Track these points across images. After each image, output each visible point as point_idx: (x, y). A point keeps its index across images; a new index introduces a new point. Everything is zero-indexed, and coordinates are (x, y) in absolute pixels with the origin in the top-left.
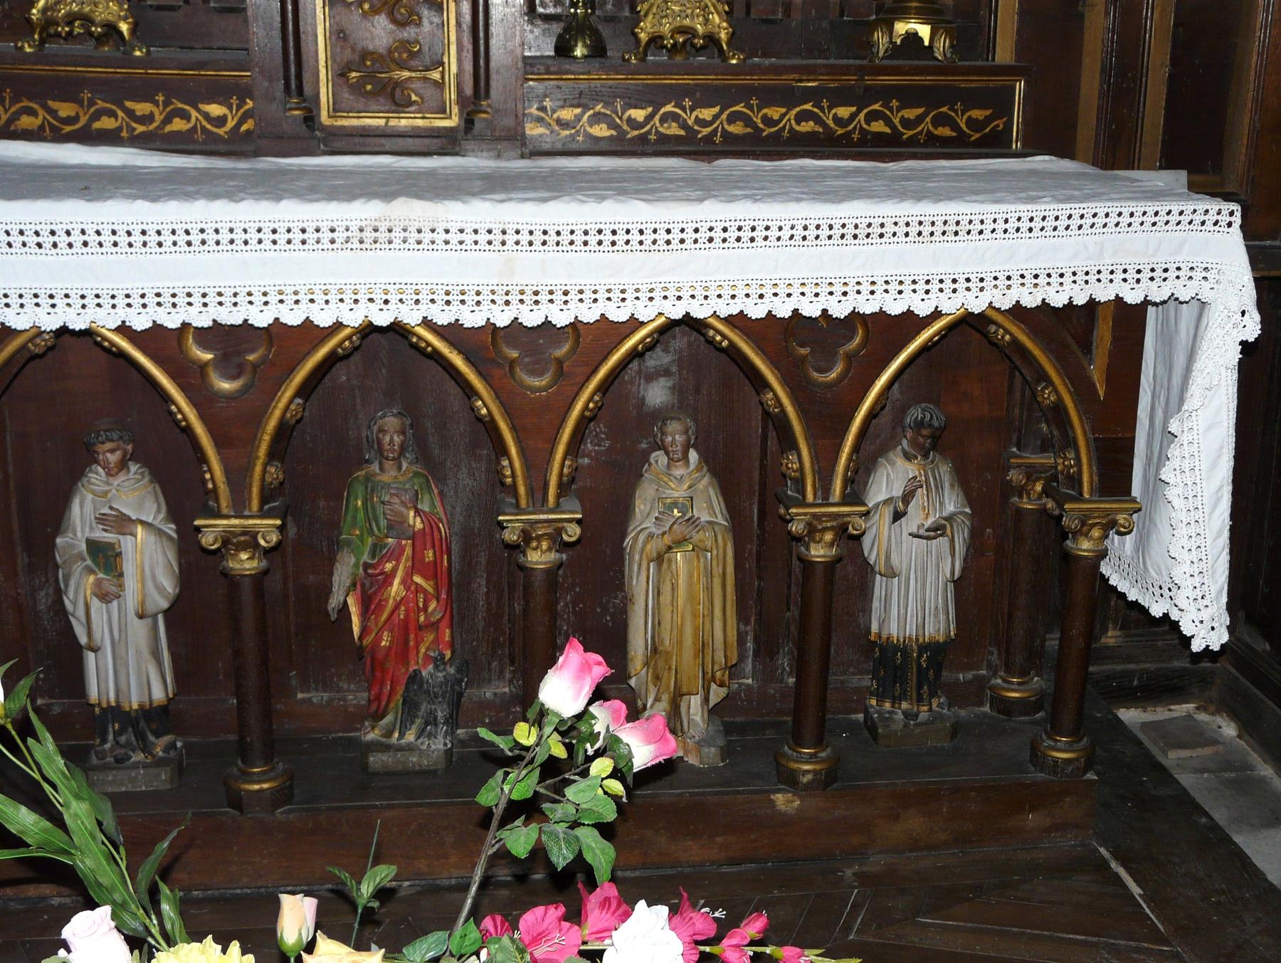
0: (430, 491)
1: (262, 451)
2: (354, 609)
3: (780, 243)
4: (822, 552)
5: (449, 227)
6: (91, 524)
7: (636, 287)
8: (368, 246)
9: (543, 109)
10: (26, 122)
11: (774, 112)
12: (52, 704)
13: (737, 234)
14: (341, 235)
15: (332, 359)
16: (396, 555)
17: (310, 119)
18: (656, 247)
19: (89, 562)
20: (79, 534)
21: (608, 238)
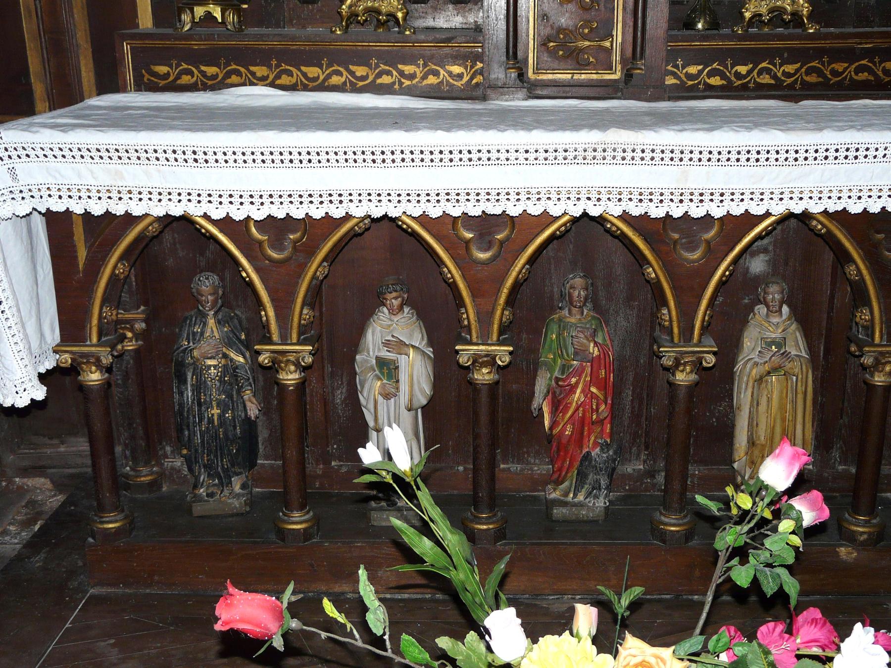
0: (602, 330)
1: (299, 301)
2: (546, 409)
3: (876, 160)
4: (883, 379)
5: (528, 149)
6: (379, 347)
7: (771, 191)
8: (589, 162)
10: (335, 80)
11: (839, 67)
12: (341, 466)
13: (846, 153)
14: (571, 154)
16: (579, 373)
17: (521, 76)
18: (787, 163)
19: (377, 372)
20: (371, 353)
21: (754, 156)
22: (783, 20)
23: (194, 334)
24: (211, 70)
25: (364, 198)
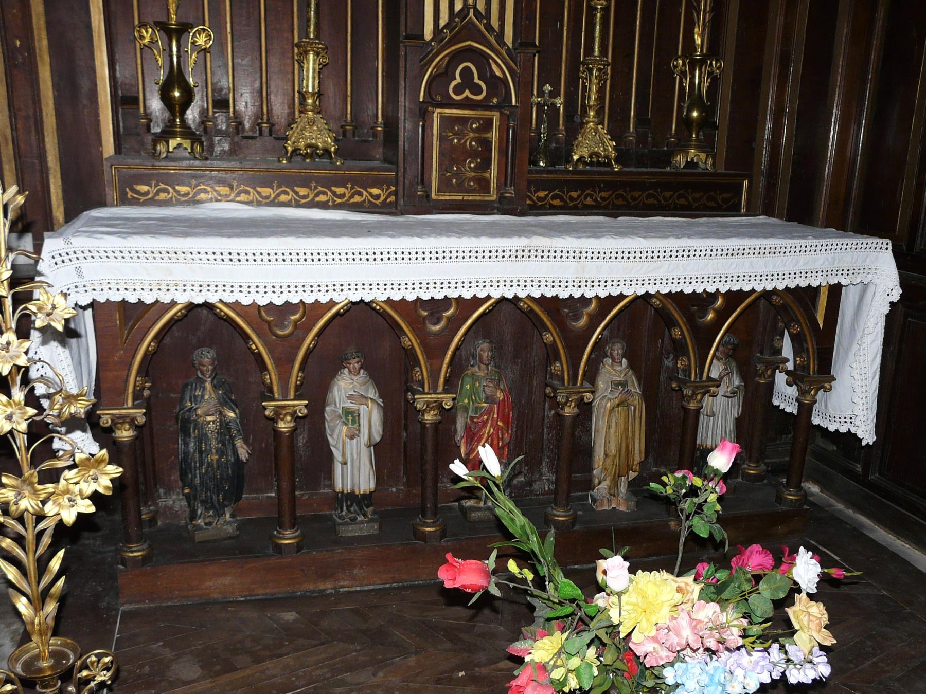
10: (283, 198)
12: (303, 494)
15: (172, 322)
19: (344, 419)
20: (338, 405)
22: (317, 154)
23: (195, 397)
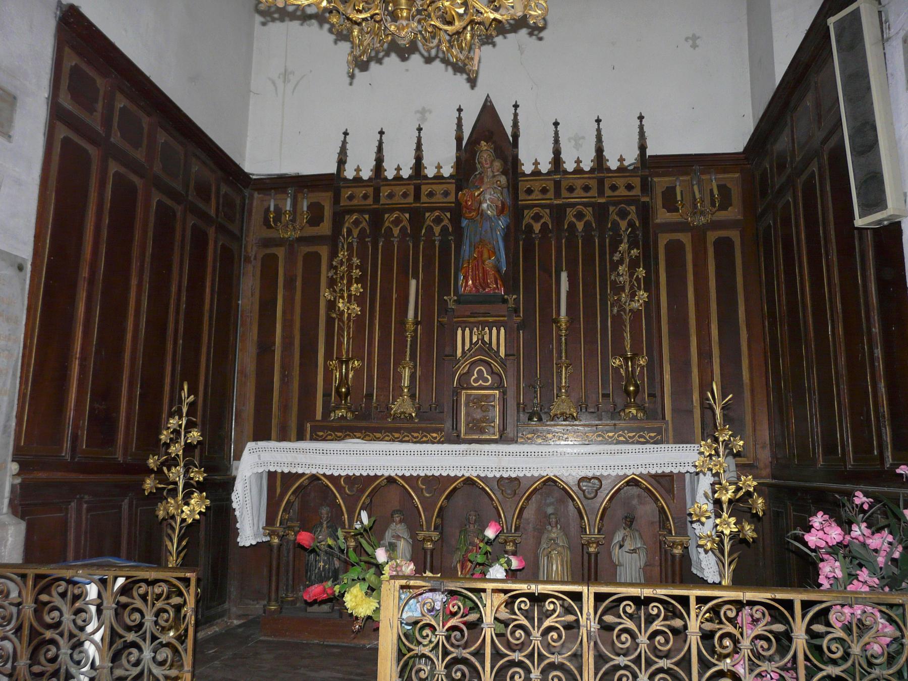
9: (523, 434)
17: (458, 436)
24: (339, 434)
25: (382, 468)
